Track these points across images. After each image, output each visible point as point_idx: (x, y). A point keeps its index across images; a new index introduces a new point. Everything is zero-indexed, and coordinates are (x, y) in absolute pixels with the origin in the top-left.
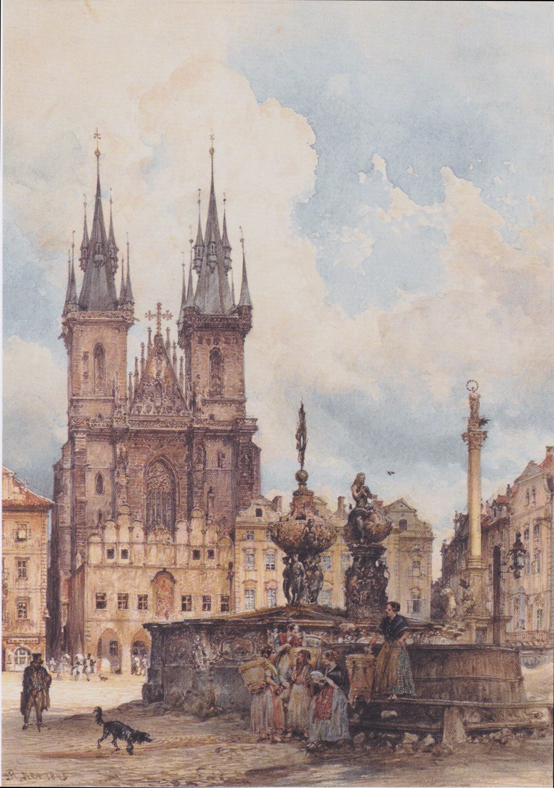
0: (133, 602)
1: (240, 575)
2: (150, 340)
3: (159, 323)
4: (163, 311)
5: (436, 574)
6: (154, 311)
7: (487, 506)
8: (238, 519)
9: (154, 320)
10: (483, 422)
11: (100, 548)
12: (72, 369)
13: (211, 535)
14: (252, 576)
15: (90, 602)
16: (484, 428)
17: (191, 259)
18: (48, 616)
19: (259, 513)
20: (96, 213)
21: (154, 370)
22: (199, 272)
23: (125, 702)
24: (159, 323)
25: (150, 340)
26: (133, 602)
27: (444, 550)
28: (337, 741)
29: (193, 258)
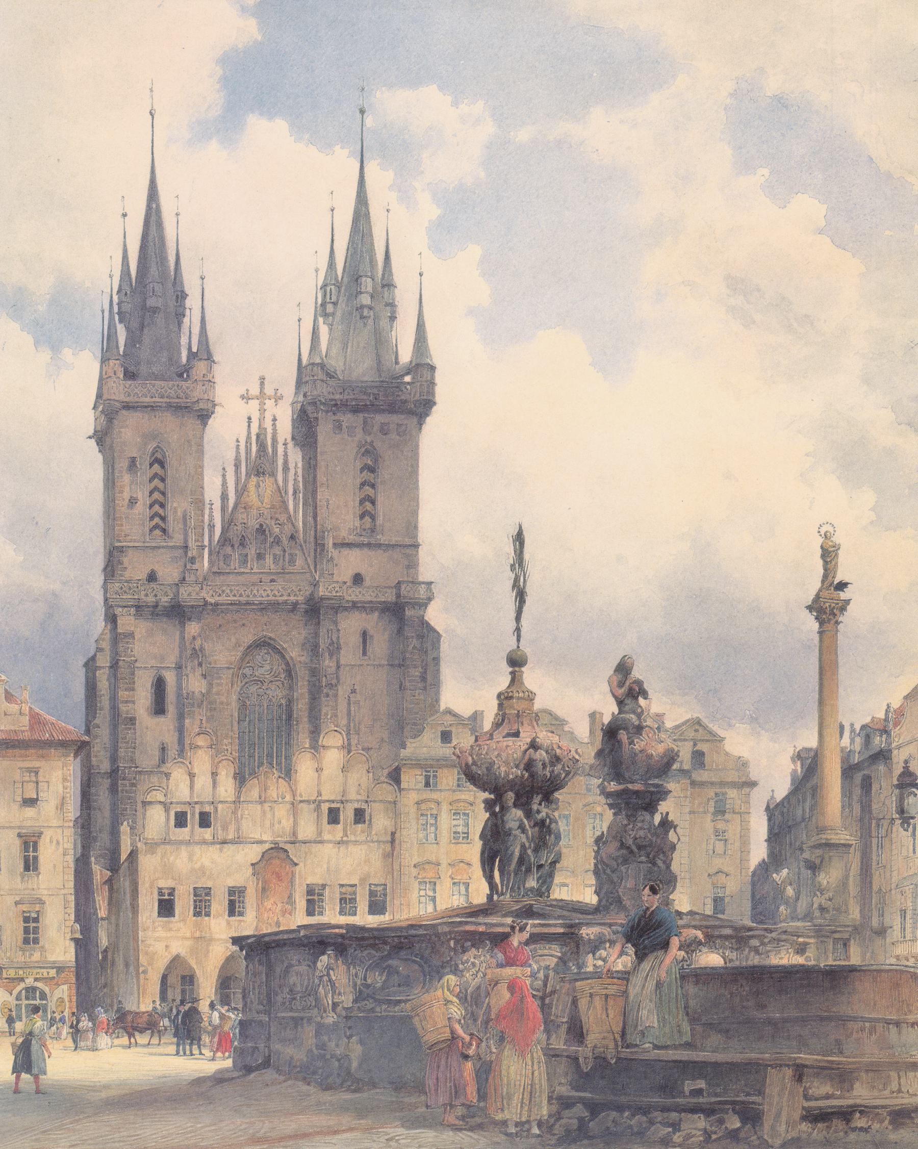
0: (219, 905)
1: (410, 855)
2: (249, 433)
3: (262, 411)
4: (269, 391)
5: (759, 852)
6: (255, 390)
7: (853, 730)
8: (404, 753)
9: (255, 404)
10: (842, 586)
11: (182, 545)
12: (110, 482)
13: (359, 779)
14: (431, 853)
15: (148, 904)
16: (843, 595)
17: (316, 303)
18: (78, 936)
19: (446, 737)
20: (149, 207)
21: (252, 496)
22: (331, 326)
23: (426, 325)
24: (262, 411)
25: (249, 433)
26: (219, 905)
27: (772, 811)
28: (633, 1115)
29: (320, 283)
